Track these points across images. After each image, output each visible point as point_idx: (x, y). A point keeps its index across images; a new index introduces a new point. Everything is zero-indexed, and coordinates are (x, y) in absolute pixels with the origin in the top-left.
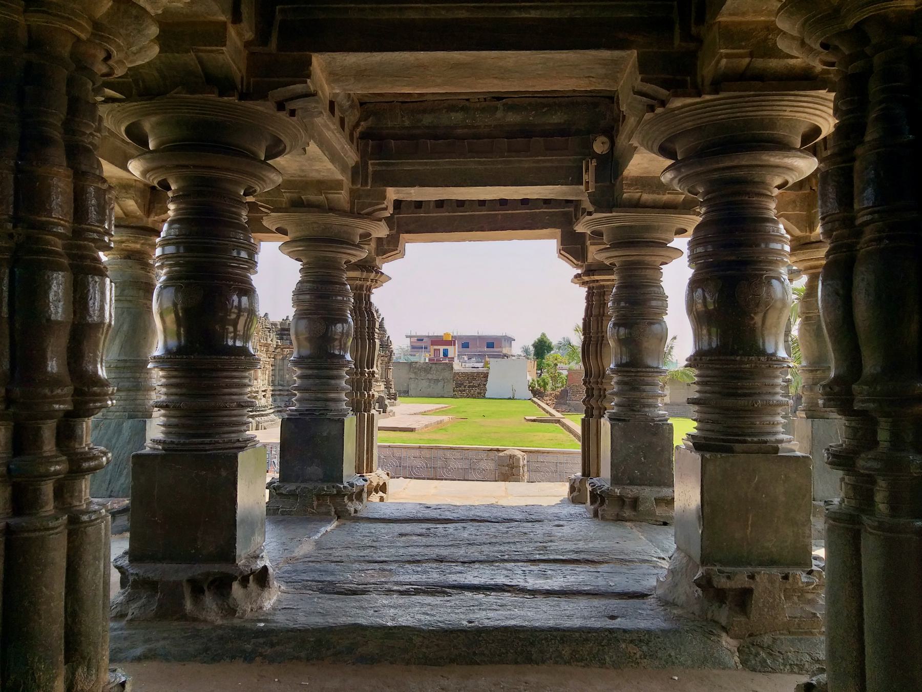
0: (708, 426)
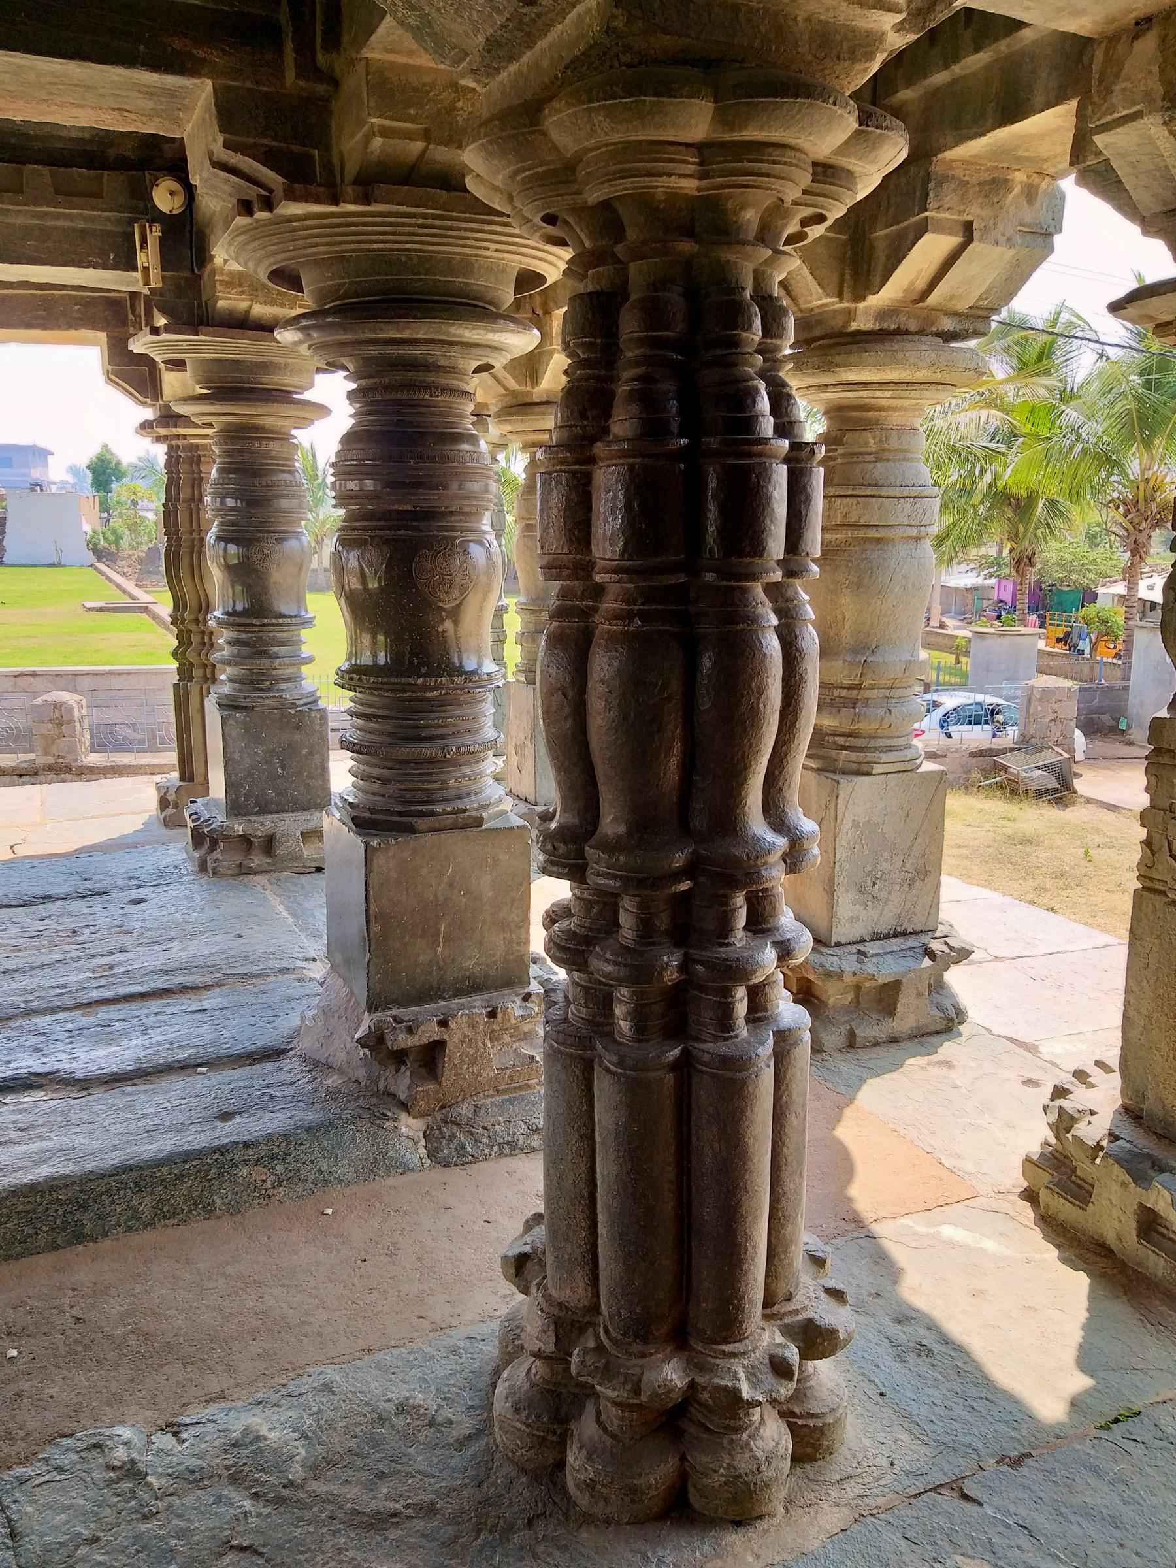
0: (375, 788)
